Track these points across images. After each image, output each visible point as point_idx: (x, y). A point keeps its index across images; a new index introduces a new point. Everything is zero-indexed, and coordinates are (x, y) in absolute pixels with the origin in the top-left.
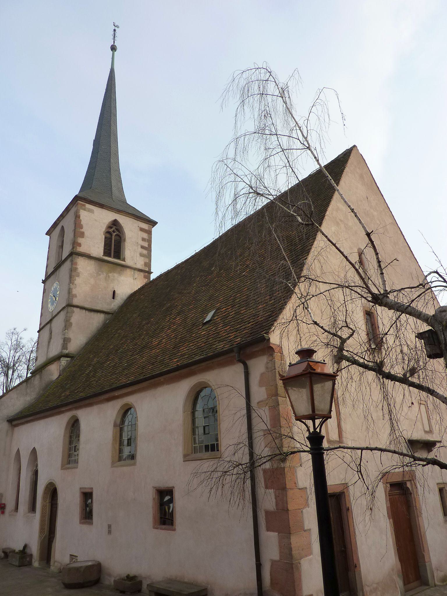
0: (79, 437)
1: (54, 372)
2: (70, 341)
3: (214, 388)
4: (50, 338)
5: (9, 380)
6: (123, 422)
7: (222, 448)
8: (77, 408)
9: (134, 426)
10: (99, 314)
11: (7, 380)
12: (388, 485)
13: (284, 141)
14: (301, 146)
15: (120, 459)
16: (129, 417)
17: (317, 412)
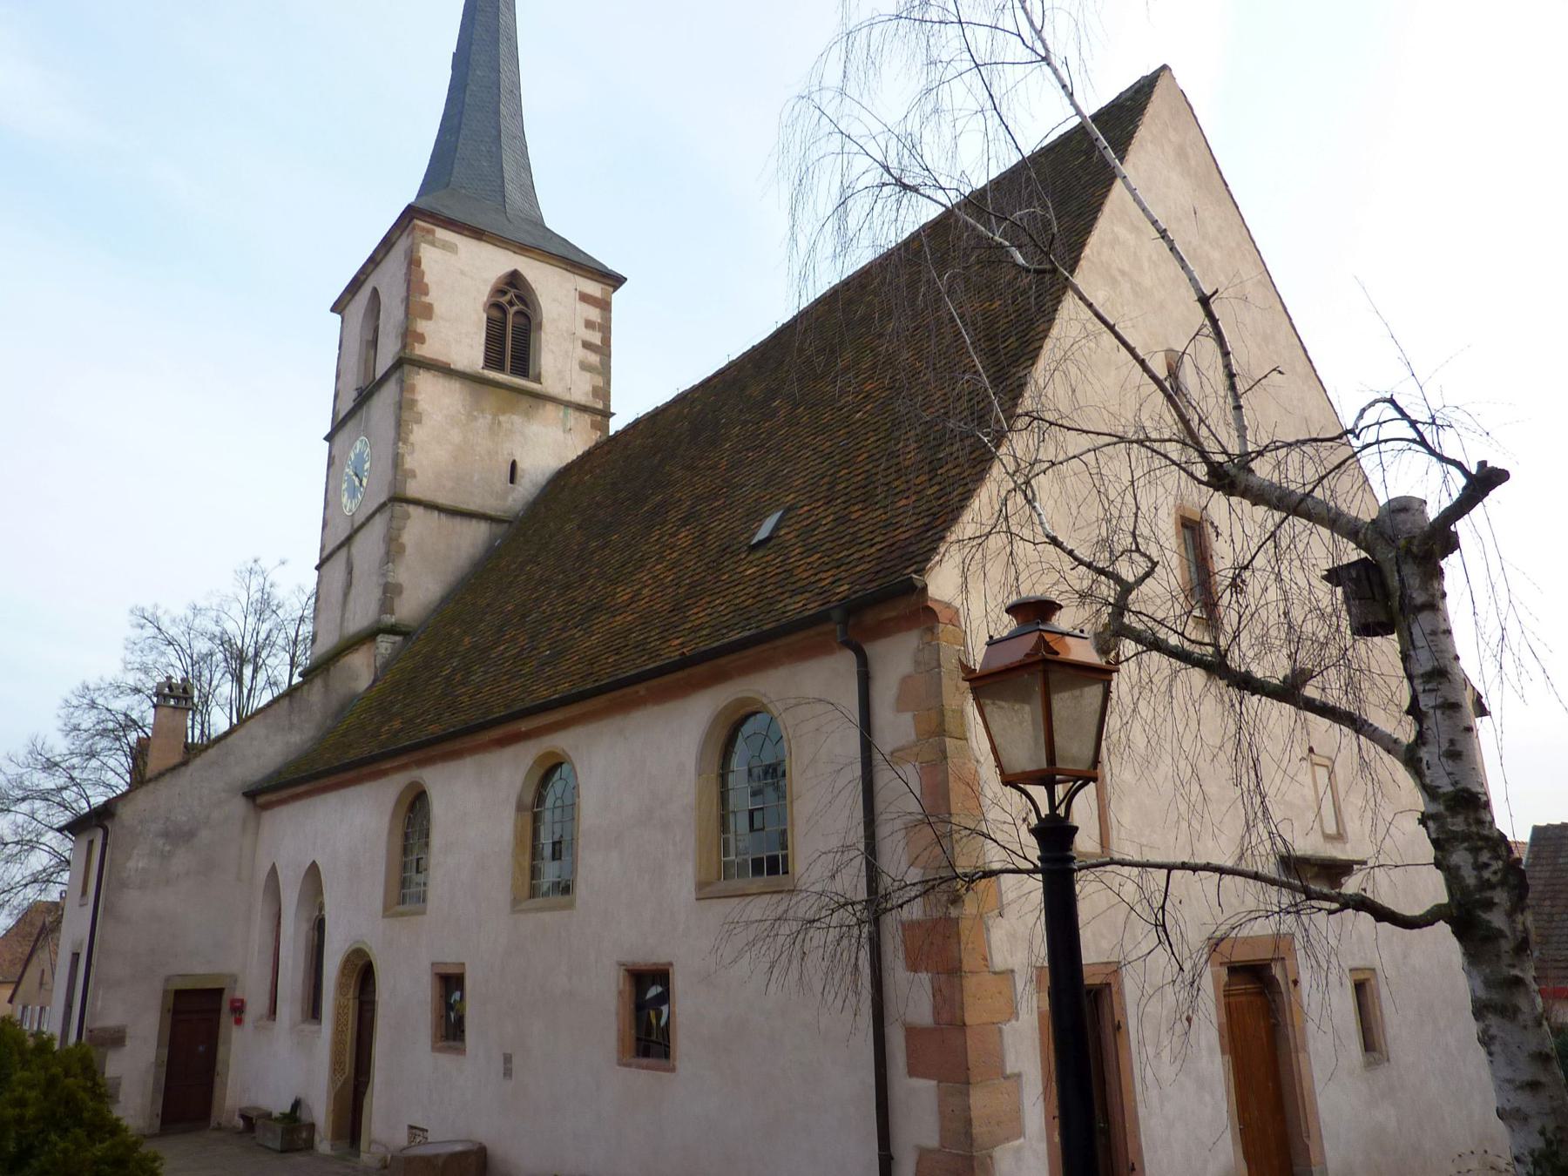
0: (427, 836)
1: (361, 670)
2: (401, 593)
3: (776, 714)
4: (349, 584)
5: (245, 691)
6: (540, 799)
7: (799, 865)
8: (422, 763)
9: (570, 809)
10: (474, 522)
11: (241, 691)
12: (1224, 971)
13: (980, 39)
14: (1027, 55)
15: (534, 892)
16: (556, 787)
17: (1059, 765)
